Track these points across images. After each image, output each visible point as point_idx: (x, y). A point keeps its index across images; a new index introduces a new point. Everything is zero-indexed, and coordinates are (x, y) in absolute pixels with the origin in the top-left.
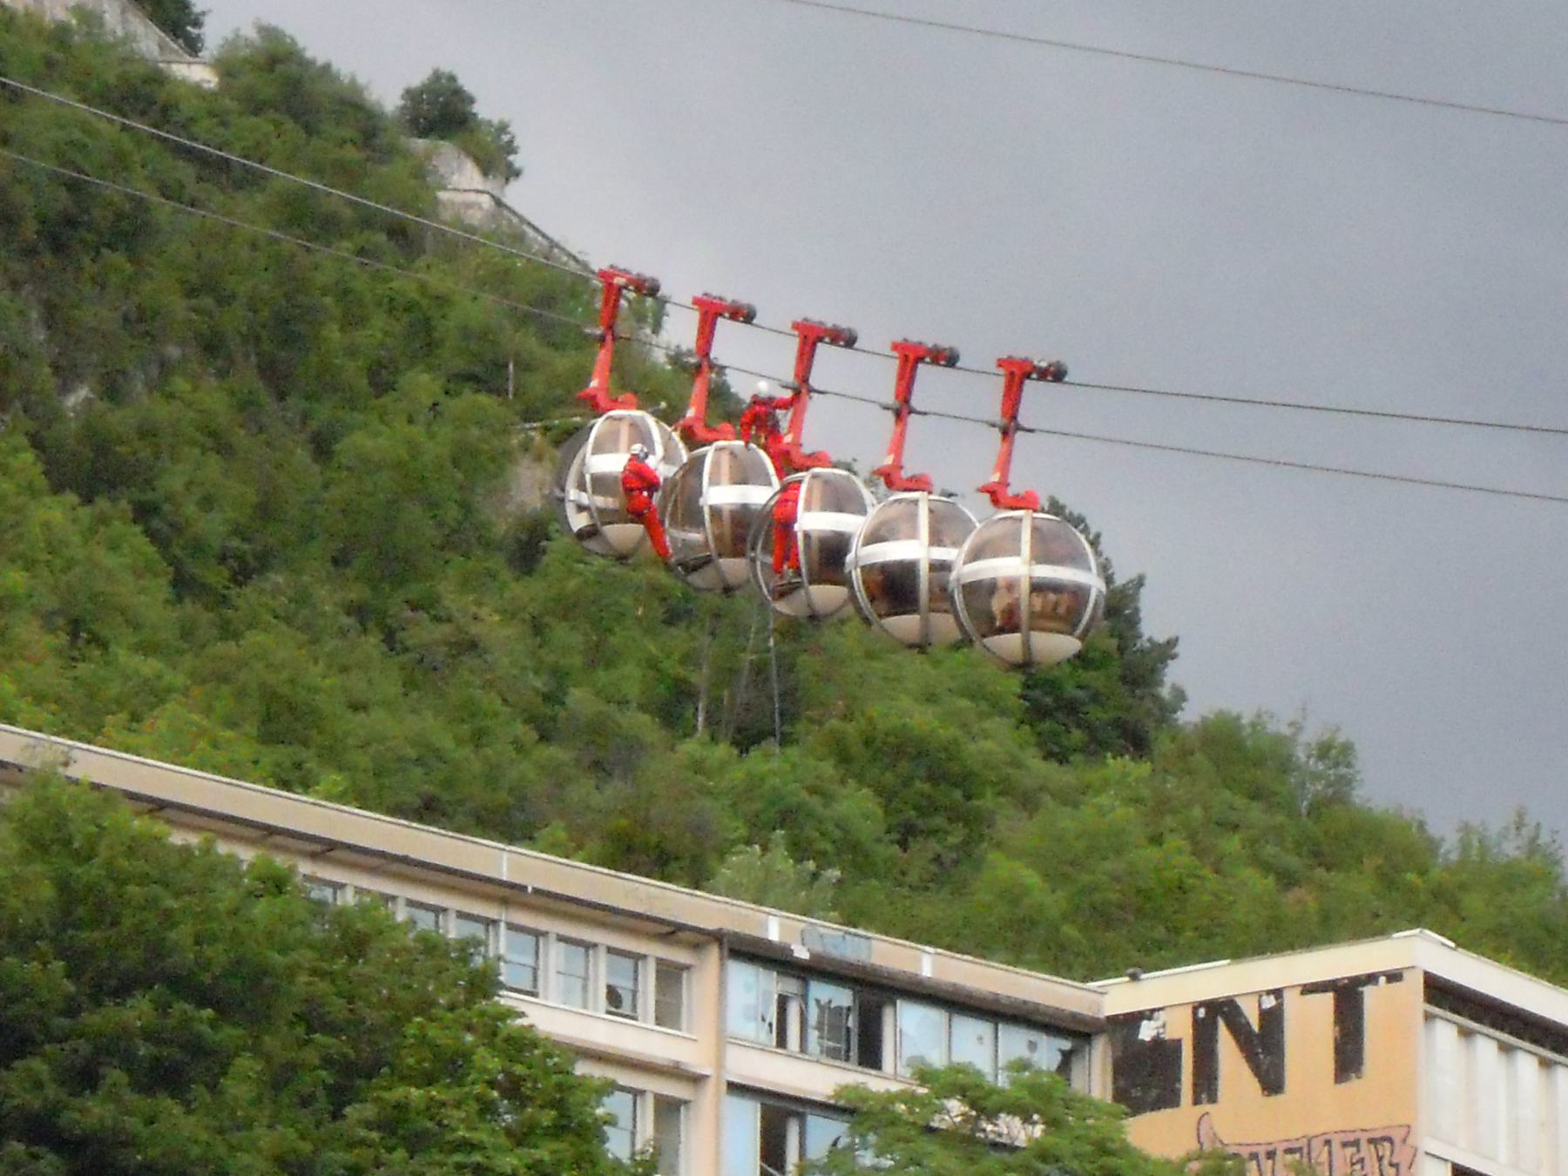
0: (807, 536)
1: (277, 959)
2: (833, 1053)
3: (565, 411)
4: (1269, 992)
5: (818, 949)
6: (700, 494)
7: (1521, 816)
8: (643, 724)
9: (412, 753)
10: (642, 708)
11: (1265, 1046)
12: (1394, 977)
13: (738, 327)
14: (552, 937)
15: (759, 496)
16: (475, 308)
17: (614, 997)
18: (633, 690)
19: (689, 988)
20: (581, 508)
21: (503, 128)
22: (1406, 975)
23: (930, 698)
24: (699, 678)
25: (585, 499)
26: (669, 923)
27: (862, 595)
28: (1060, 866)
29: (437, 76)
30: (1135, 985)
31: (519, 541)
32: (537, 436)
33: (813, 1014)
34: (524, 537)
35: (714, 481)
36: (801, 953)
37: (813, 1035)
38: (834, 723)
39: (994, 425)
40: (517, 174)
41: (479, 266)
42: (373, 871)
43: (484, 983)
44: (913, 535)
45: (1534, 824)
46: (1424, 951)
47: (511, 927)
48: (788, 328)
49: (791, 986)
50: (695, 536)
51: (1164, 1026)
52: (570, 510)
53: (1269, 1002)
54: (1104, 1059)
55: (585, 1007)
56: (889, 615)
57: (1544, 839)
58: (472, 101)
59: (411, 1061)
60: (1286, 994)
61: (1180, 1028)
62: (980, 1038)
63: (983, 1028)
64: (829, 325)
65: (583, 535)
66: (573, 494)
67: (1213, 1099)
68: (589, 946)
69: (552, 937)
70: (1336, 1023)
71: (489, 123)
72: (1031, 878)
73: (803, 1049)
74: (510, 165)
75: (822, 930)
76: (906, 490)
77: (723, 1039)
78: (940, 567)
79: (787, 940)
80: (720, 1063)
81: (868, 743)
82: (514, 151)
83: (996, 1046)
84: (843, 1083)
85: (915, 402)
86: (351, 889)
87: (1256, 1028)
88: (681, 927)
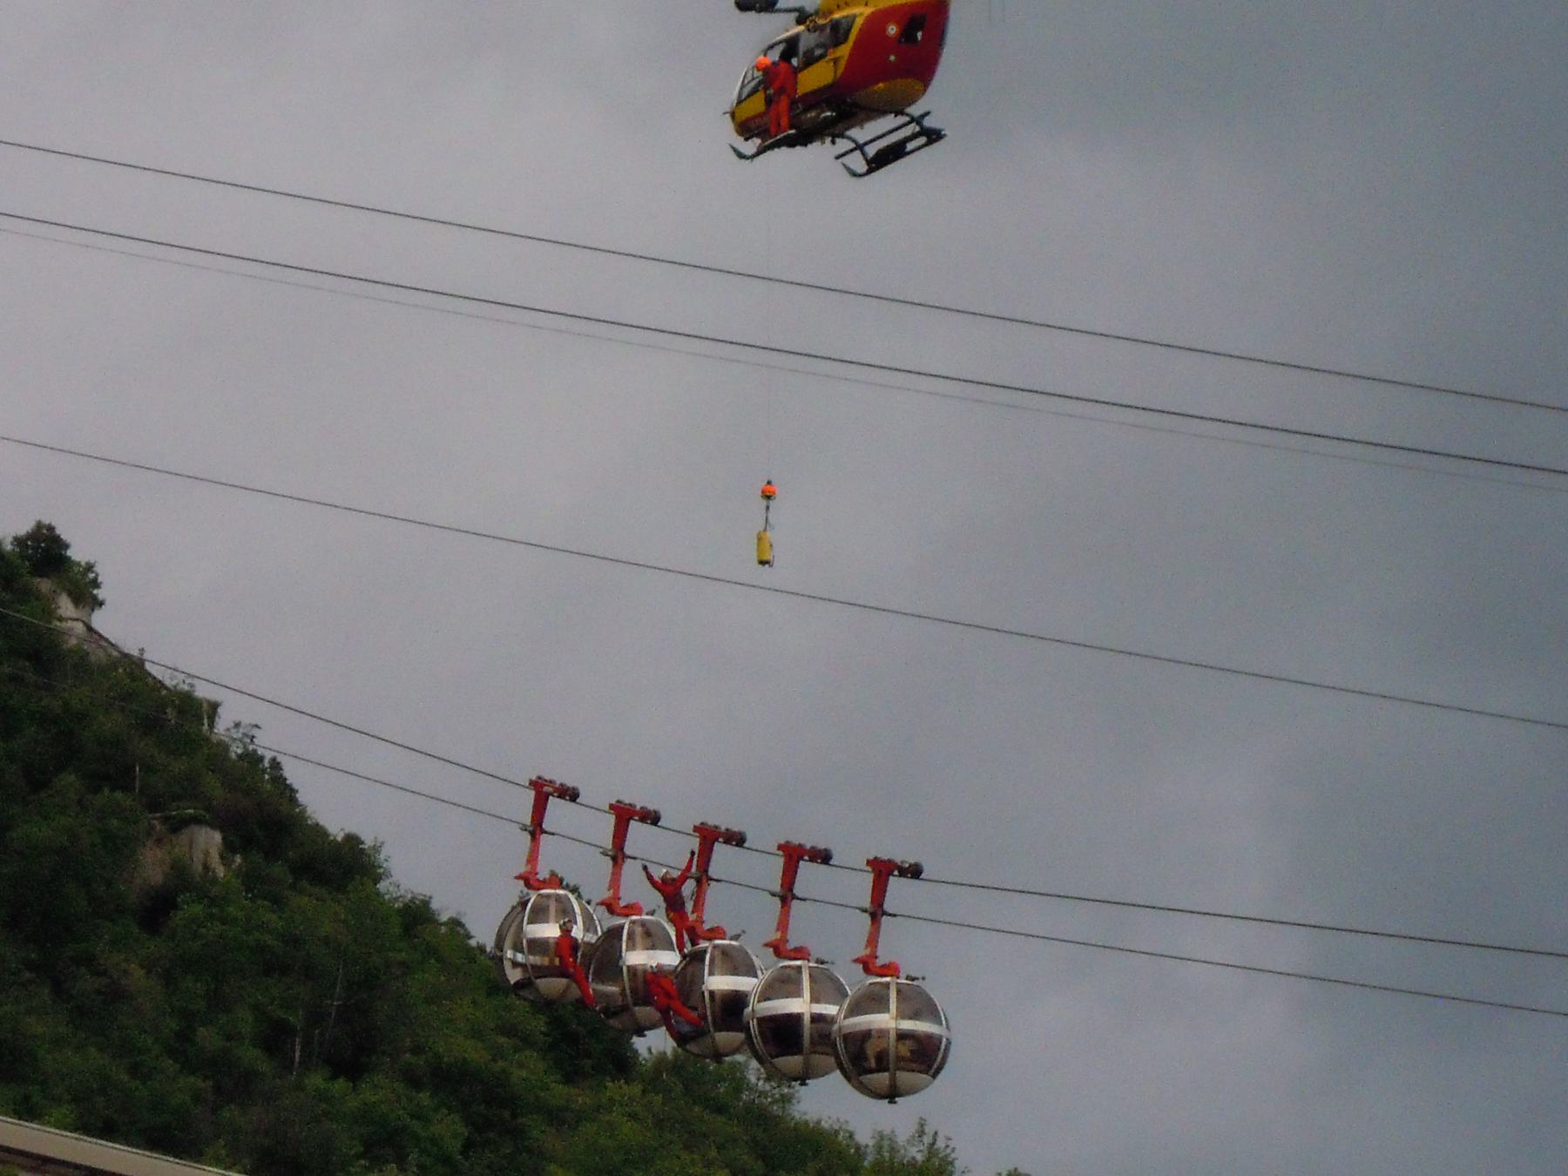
0: (712, 993)
7: (922, 1125)
8: (250, 1055)
13: (646, 828)
15: (669, 959)
16: (111, 723)
20: (515, 964)
21: (90, 567)
23: (476, 1034)
24: (296, 1019)
25: (520, 958)
27: (758, 1041)
29: (39, 525)
35: (632, 946)
40: (101, 604)
41: (110, 689)
44: (798, 993)
48: (774, 849)
50: (613, 989)
52: (507, 965)
57: (940, 1144)
58: (67, 546)
65: (520, 985)
66: (509, 954)
71: (79, 564)
74: (95, 598)
78: (817, 1018)
85: (887, 906)
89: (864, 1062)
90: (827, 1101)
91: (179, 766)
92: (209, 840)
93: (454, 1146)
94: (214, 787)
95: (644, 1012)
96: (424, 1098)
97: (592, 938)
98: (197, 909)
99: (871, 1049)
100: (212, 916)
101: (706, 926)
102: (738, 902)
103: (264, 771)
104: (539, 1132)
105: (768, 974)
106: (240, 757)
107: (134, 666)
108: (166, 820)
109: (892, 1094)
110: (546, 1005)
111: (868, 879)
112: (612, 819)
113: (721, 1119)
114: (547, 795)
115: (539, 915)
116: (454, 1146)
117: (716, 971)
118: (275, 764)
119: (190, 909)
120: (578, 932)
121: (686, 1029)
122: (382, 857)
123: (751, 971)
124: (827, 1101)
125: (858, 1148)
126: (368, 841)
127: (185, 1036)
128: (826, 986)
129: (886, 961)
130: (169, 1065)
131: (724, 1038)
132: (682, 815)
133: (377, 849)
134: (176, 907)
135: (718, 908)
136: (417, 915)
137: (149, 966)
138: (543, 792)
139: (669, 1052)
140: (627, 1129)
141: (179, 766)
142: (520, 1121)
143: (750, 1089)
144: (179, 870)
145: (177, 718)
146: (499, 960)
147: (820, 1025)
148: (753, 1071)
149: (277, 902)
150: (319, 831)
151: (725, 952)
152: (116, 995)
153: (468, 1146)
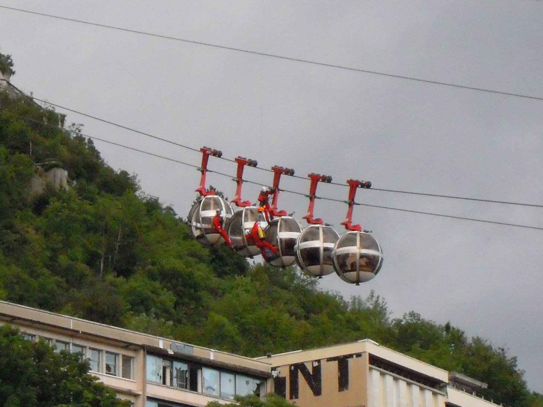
1: (21, 362)
2: (181, 386)
3: (50, 159)
4: (316, 361)
5: (176, 351)
6: (242, 225)
8: (82, 267)
9: (15, 281)
10: (82, 262)
11: (314, 379)
12: (359, 355)
14: (104, 352)
16: (18, 125)
17: (108, 368)
18: (80, 256)
19: (133, 364)
20: (197, 228)
21: (8, 57)
22: (363, 354)
23: (180, 257)
24: (101, 251)
25: (199, 225)
26: (126, 343)
27: (301, 260)
28: (234, 316)
30: (270, 358)
31: (35, 204)
32: (40, 167)
33: (175, 373)
34: (37, 203)
36: (171, 352)
37: (175, 380)
38: (150, 267)
39: (346, 202)
40: (14, 73)
42: (96, 342)
43: (84, 367)
45: (377, 296)
46: (371, 347)
47: (107, 352)
49: (167, 363)
51: (280, 372)
52: (193, 229)
53: (316, 364)
54: (272, 384)
55: (99, 372)
56: (309, 265)
57: (380, 301)
59: (62, 395)
60: (322, 361)
61: (285, 373)
62: (230, 380)
63: (230, 377)
64: (284, 168)
65: (198, 237)
66: (194, 224)
67: (297, 397)
68: (100, 351)
69: (88, 348)
70: (339, 371)
71: (4, 56)
72: (225, 320)
73: (171, 384)
74: (11, 70)
75: (177, 344)
76: (314, 224)
77: (145, 382)
78: (326, 249)
79: (166, 348)
80: (144, 390)
81: (161, 274)
82: (12, 65)
83: (235, 382)
84: (210, 401)
85: (317, 194)
86: (38, 335)
87: (311, 373)
88: (131, 344)
89: (344, 266)
90: (331, 284)
91: (48, 143)
92: (62, 174)
93: (170, 305)
94: (64, 151)
95: (253, 248)
96: (157, 284)
97: (230, 216)
98: (58, 204)
99: (349, 262)
100: (64, 207)
101: (278, 211)
102: (291, 201)
103: (85, 144)
104: (206, 297)
105: (304, 230)
106: (75, 138)
107: (29, 100)
108: (43, 166)
109: (357, 281)
110: (212, 246)
111: (348, 189)
112: (273, 174)
113: (285, 292)
114: (208, 155)
115: (206, 207)
116: (170, 305)
117: (282, 230)
118: (90, 142)
119: (54, 204)
120: (223, 214)
121: (270, 255)
122: (137, 180)
123: (298, 230)
124: (331, 284)
125: (345, 303)
126: (131, 174)
127: (53, 259)
128: (330, 235)
129: (355, 224)
130: (46, 271)
131: (287, 259)
132: (267, 162)
133: (134, 177)
134: (48, 203)
135: (283, 202)
136: (152, 206)
137: (37, 230)
138: (206, 153)
139: (262, 263)
140: (244, 296)
141: (48, 143)
142: (199, 293)
143: (299, 278)
144: (50, 189)
145: (47, 122)
146: (188, 224)
147: (327, 252)
148: (298, 271)
149: (92, 201)
150: (110, 170)
151: (286, 221)
152: (24, 242)
153: (176, 305)
